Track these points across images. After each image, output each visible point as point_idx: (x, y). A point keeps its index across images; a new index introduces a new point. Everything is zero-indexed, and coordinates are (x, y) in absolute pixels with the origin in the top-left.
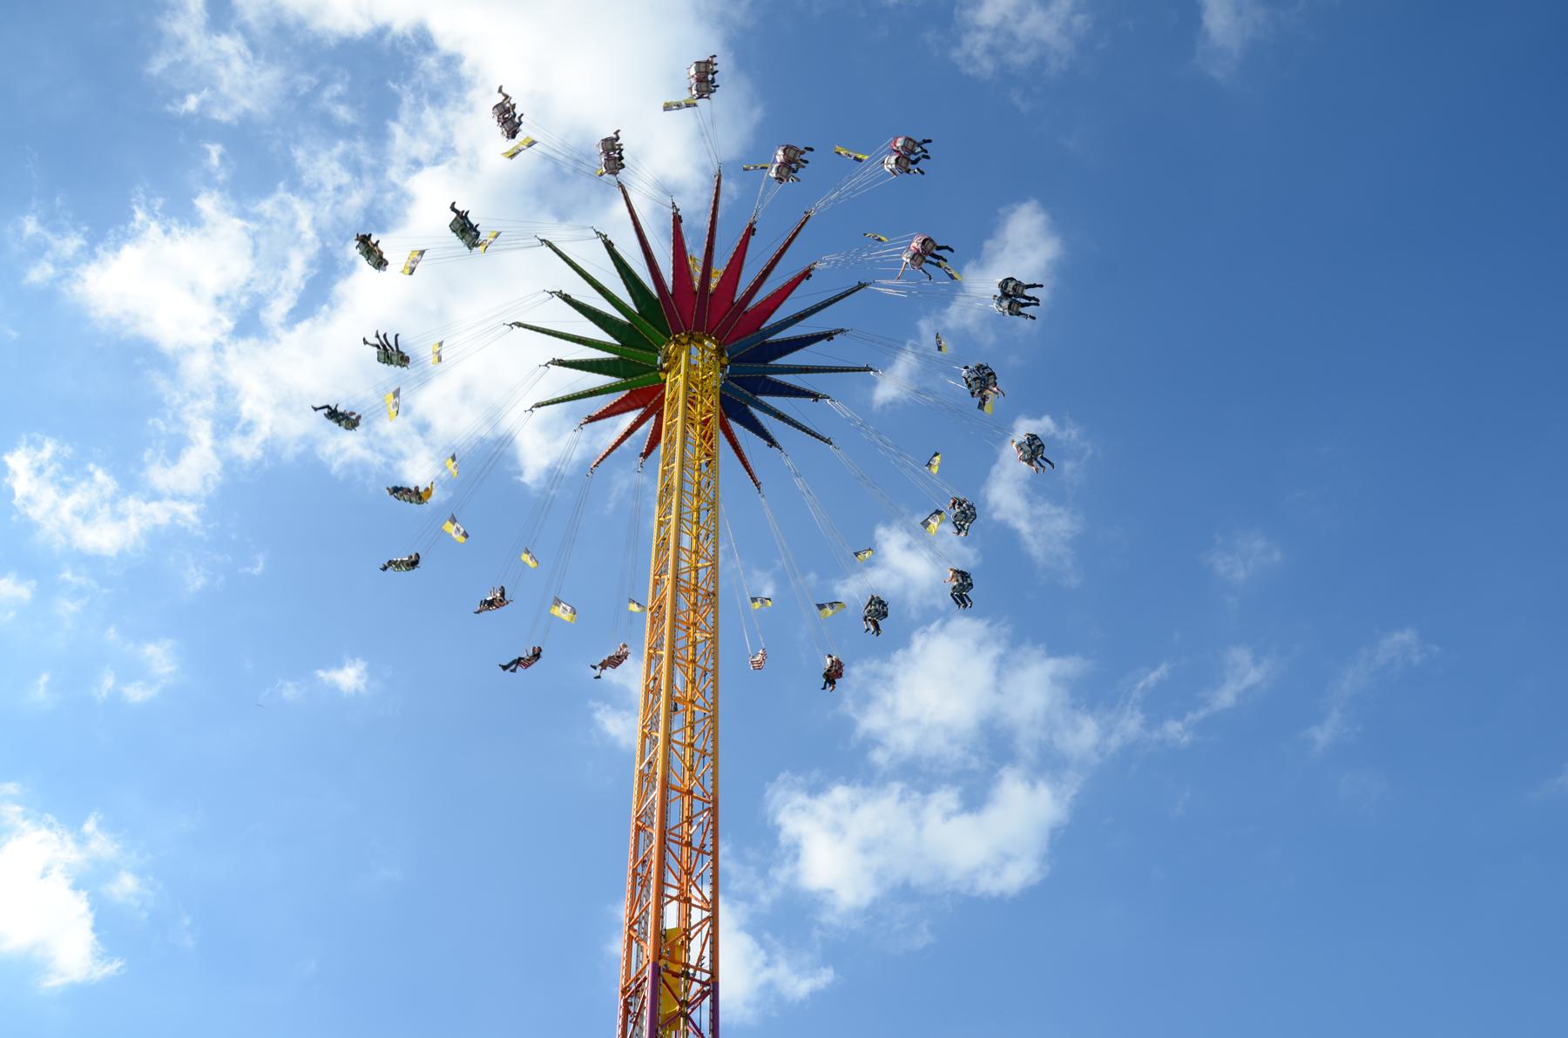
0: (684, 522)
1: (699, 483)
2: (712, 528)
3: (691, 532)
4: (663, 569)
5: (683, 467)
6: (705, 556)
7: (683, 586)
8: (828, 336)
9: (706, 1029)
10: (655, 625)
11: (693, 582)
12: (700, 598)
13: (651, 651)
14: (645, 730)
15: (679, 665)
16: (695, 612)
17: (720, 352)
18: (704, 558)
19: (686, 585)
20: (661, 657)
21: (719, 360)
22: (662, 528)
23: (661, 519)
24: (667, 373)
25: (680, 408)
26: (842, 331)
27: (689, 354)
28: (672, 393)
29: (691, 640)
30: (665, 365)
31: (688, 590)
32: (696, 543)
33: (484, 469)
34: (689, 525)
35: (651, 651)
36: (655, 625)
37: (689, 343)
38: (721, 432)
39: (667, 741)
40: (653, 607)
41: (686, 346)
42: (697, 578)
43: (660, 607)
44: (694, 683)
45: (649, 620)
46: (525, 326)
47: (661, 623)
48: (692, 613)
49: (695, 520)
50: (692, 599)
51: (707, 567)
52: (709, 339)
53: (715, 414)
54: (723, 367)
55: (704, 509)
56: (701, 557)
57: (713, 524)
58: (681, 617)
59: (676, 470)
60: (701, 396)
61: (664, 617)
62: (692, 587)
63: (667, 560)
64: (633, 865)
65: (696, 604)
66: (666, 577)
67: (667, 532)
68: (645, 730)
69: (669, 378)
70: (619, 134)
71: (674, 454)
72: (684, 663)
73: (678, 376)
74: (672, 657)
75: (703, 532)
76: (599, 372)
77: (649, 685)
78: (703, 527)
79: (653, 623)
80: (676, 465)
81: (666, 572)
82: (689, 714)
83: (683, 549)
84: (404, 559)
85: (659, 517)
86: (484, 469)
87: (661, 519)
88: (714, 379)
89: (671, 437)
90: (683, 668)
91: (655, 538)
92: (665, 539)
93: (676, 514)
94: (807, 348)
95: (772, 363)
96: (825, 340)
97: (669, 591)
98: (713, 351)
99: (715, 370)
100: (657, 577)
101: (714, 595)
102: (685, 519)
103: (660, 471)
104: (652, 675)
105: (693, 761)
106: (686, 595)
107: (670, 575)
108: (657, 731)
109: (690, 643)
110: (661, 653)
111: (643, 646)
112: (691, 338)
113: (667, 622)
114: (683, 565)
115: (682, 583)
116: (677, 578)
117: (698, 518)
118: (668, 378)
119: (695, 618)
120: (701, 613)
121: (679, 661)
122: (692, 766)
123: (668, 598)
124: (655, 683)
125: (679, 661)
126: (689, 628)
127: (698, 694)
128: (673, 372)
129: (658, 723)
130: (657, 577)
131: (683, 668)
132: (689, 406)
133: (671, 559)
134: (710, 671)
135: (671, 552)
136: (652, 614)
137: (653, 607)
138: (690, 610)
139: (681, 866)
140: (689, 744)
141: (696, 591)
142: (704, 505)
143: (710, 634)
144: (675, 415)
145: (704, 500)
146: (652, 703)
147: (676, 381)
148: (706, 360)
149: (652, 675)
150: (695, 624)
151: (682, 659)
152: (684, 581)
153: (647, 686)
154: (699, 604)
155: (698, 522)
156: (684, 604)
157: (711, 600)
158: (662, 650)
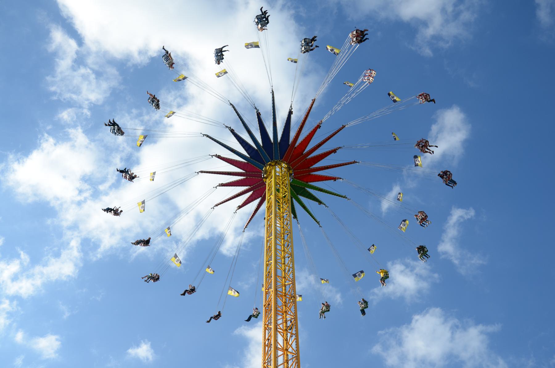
0: (278, 263)
1: (284, 245)
2: (291, 266)
3: (282, 268)
4: (270, 235)
5: (276, 237)
6: (288, 279)
7: (279, 294)
8: (334, 151)
9: (294, 367)
10: (267, 313)
11: (284, 292)
12: (287, 299)
13: (266, 326)
14: (265, 365)
15: (280, 332)
16: (286, 306)
17: (289, 169)
18: (288, 280)
19: (280, 293)
20: (271, 328)
21: (289, 172)
22: (268, 243)
23: (267, 263)
24: (266, 179)
25: (273, 191)
26: (340, 148)
27: (275, 171)
28: (269, 204)
29: (284, 319)
30: (265, 176)
31: (282, 296)
32: (284, 273)
33: (235, 82)
34: (280, 264)
35: (266, 326)
36: (267, 313)
37: (275, 165)
38: (292, 214)
39: (276, 328)
40: (266, 305)
41: (274, 167)
42: (285, 290)
43: (269, 305)
44: (287, 340)
45: (264, 311)
46: (205, 172)
47: (270, 312)
48: (284, 307)
49: (283, 262)
50: (284, 300)
51: (290, 284)
52: (284, 163)
53: (288, 192)
54: (290, 175)
55: (287, 257)
56: (287, 280)
57: (289, 218)
58: (279, 309)
59: (273, 240)
60: (283, 204)
61: (271, 309)
62: (283, 294)
63: (271, 282)
64: (264, 342)
65: (285, 302)
66: (271, 290)
67: (271, 269)
68: (265, 365)
69: (268, 181)
70: (183, 292)
71: (271, 232)
72: (281, 331)
73: (271, 196)
74: (276, 329)
75: (287, 268)
76: (244, 147)
77: (265, 342)
78: (287, 266)
79: (266, 312)
80: (273, 237)
81: (271, 288)
82: (285, 356)
83: (278, 276)
84: (153, 281)
85: (266, 262)
86: (235, 82)
87: (267, 263)
88: (288, 180)
89: (270, 224)
90: (281, 333)
91: (265, 272)
92: (270, 247)
93: (274, 236)
94: (325, 158)
95: (312, 167)
96: (333, 153)
97: (273, 297)
98: (286, 168)
99: (287, 176)
100: (267, 290)
101: (294, 297)
102: (278, 262)
103: (265, 264)
104: (267, 337)
105: (287, 337)
106: (280, 298)
107: (273, 289)
108: (271, 365)
109: (284, 321)
110: (270, 326)
111: (268, 154)
112: (276, 163)
113: (273, 311)
114: (279, 284)
115: (279, 293)
116: (276, 290)
117: (284, 261)
118: (267, 181)
119: (286, 309)
120: (288, 306)
121: (279, 330)
122: (287, 339)
123: (273, 300)
124: (268, 341)
125: (279, 330)
126: (283, 314)
127: (287, 309)
128: (269, 178)
129: (271, 361)
130: (267, 290)
131: (281, 333)
132: (277, 200)
133: (273, 281)
134: (294, 334)
135: (273, 278)
136: (265, 308)
137: (266, 305)
138: (283, 305)
139: (284, 338)
140: (285, 330)
141: (286, 296)
142: (287, 255)
143: (293, 316)
144: (271, 194)
145: (287, 253)
146: (268, 352)
147: (270, 198)
148: (283, 173)
149: (267, 337)
150: (286, 312)
151: (281, 329)
152: (280, 292)
153: (265, 343)
154: (287, 303)
155: (284, 263)
156: (280, 302)
157: (293, 300)
158: (271, 325)
